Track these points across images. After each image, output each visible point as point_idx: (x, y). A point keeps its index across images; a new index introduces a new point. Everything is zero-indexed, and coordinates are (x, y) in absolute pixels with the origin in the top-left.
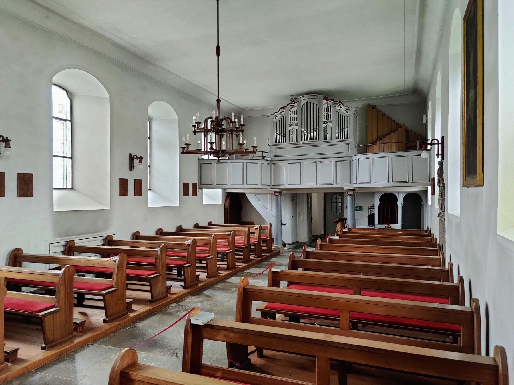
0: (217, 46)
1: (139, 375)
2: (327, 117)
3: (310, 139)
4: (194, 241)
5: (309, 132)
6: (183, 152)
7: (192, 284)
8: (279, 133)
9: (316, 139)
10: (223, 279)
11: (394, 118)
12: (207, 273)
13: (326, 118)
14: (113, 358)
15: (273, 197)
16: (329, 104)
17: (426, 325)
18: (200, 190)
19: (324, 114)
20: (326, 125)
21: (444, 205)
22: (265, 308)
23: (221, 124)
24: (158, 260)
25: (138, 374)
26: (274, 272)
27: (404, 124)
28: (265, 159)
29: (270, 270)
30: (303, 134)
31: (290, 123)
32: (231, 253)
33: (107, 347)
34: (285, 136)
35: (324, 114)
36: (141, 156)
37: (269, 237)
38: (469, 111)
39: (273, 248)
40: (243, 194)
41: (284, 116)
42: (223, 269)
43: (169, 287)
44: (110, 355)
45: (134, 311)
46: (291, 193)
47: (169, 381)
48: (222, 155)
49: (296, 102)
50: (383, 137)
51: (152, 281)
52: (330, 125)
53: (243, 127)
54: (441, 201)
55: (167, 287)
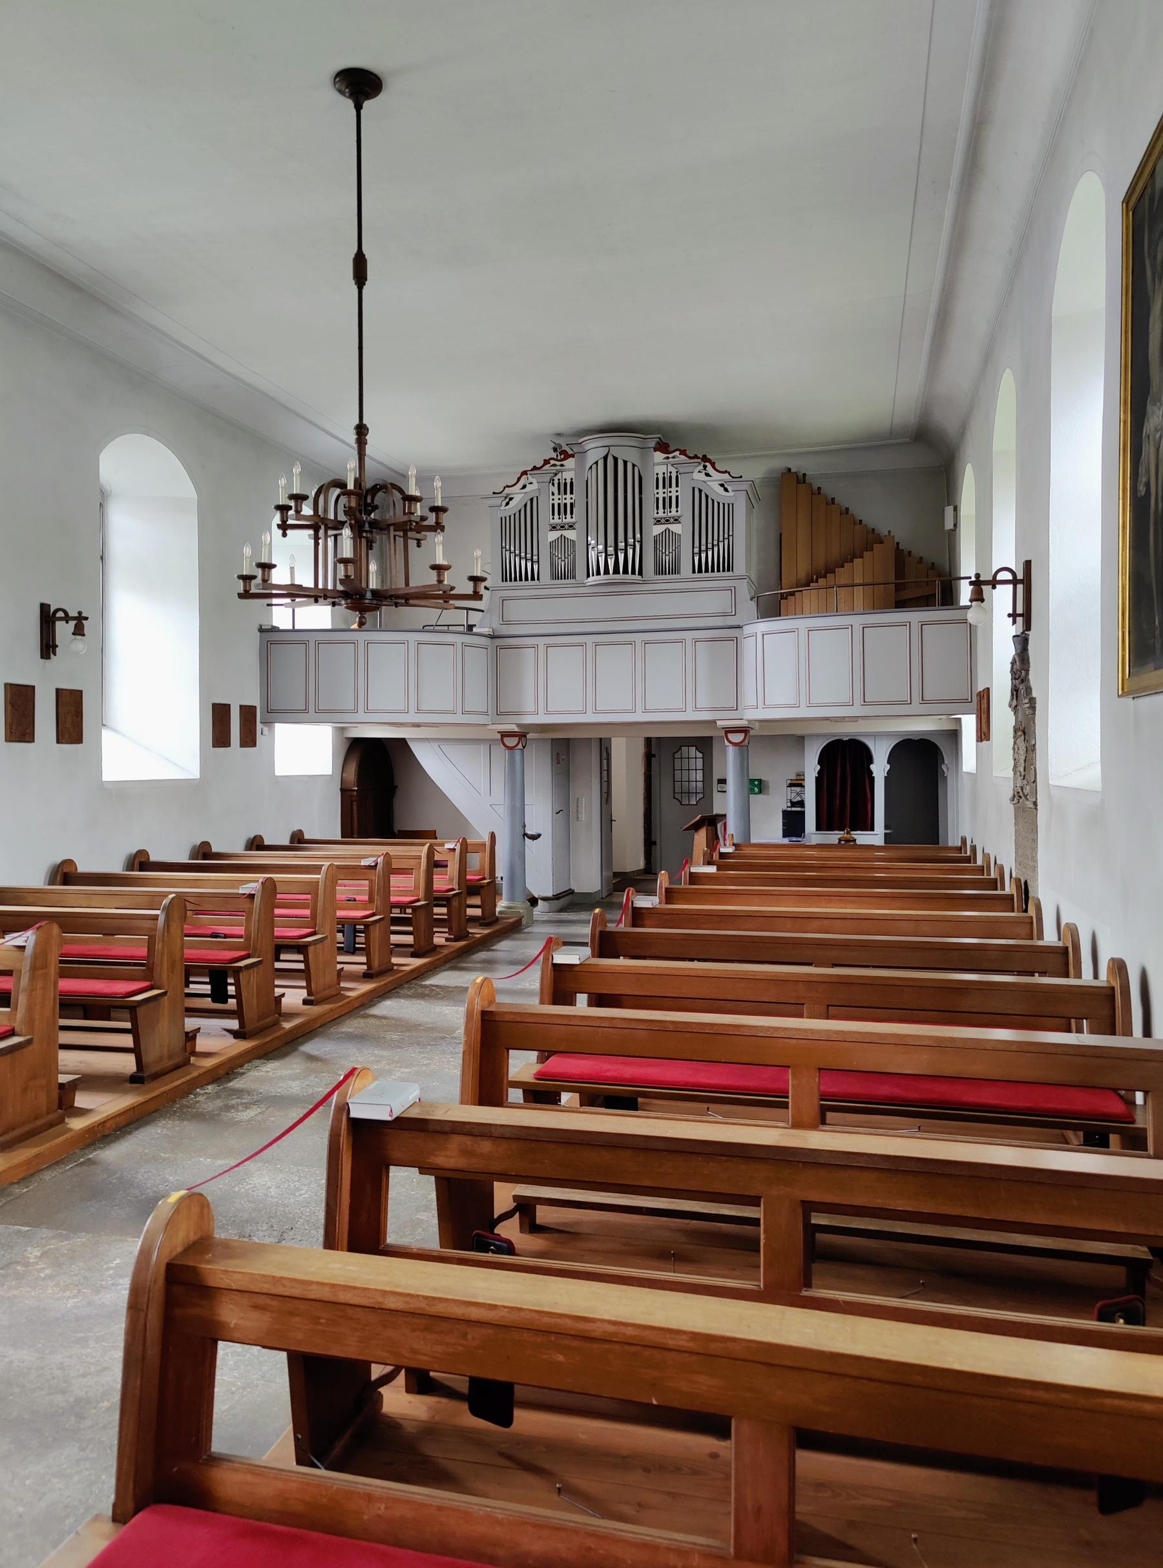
0: (356, 255)
1: (235, 1272)
2: (667, 503)
3: (616, 571)
4: (270, 888)
5: (612, 549)
6: (246, 591)
7: (262, 1023)
8: (517, 552)
9: (633, 572)
10: (356, 1008)
11: (859, 512)
12: (305, 991)
13: (664, 508)
14: (34, 1263)
15: (500, 753)
16: (672, 465)
17: (1029, 1105)
18: (266, 730)
19: (658, 493)
20: (664, 530)
21: (1033, 764)
22: (536, 1079)
23: (369, 505)
24: (159, 946)
25: (231, 1270)
26: (557, 967)
27: (889, 532)
28: (475, 630)
29: (546, 959)
30: (592, 554)
31: (553, 519)
32: (377, 925)
33: (6, 1228)
34: (538, 562)
35: (657, 496)
36: (80, 613)
37: (487, 875)
38: (1142, 470)
39: (501, 912)
40: (402, 743)
41: (535, 499)
42: (353, 977)
43: (190, 1035)
44: (25, 1253)
45: (83, 1112)
46: (552, 739)
47: (342, 1283)
48: (375, 602)
49: (572, 456)
50: (829, 570)
51: (141, 1012)
52: (675, 528)
53: (441, 514)
54: (1022, 752)
55: (187, 1033)
